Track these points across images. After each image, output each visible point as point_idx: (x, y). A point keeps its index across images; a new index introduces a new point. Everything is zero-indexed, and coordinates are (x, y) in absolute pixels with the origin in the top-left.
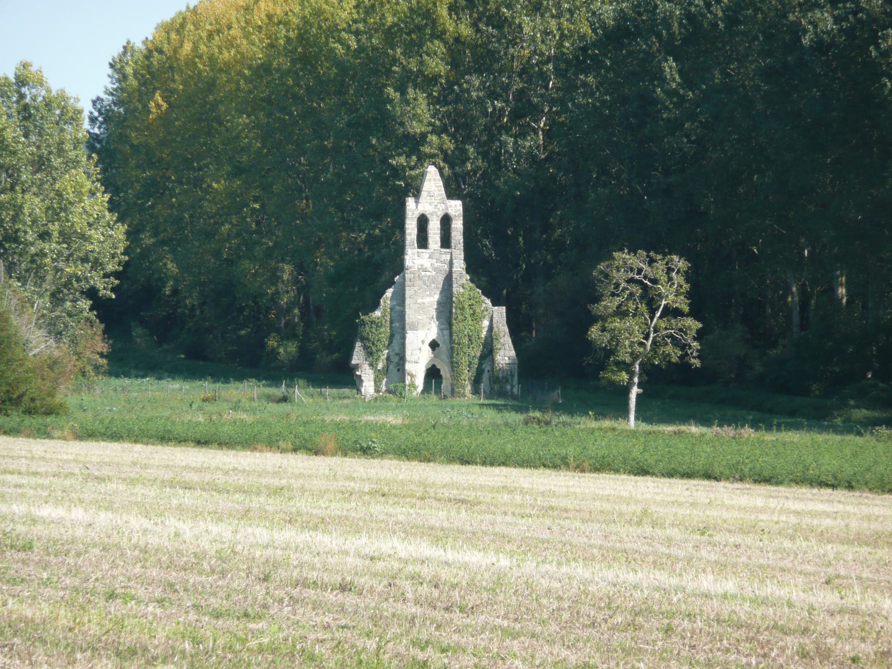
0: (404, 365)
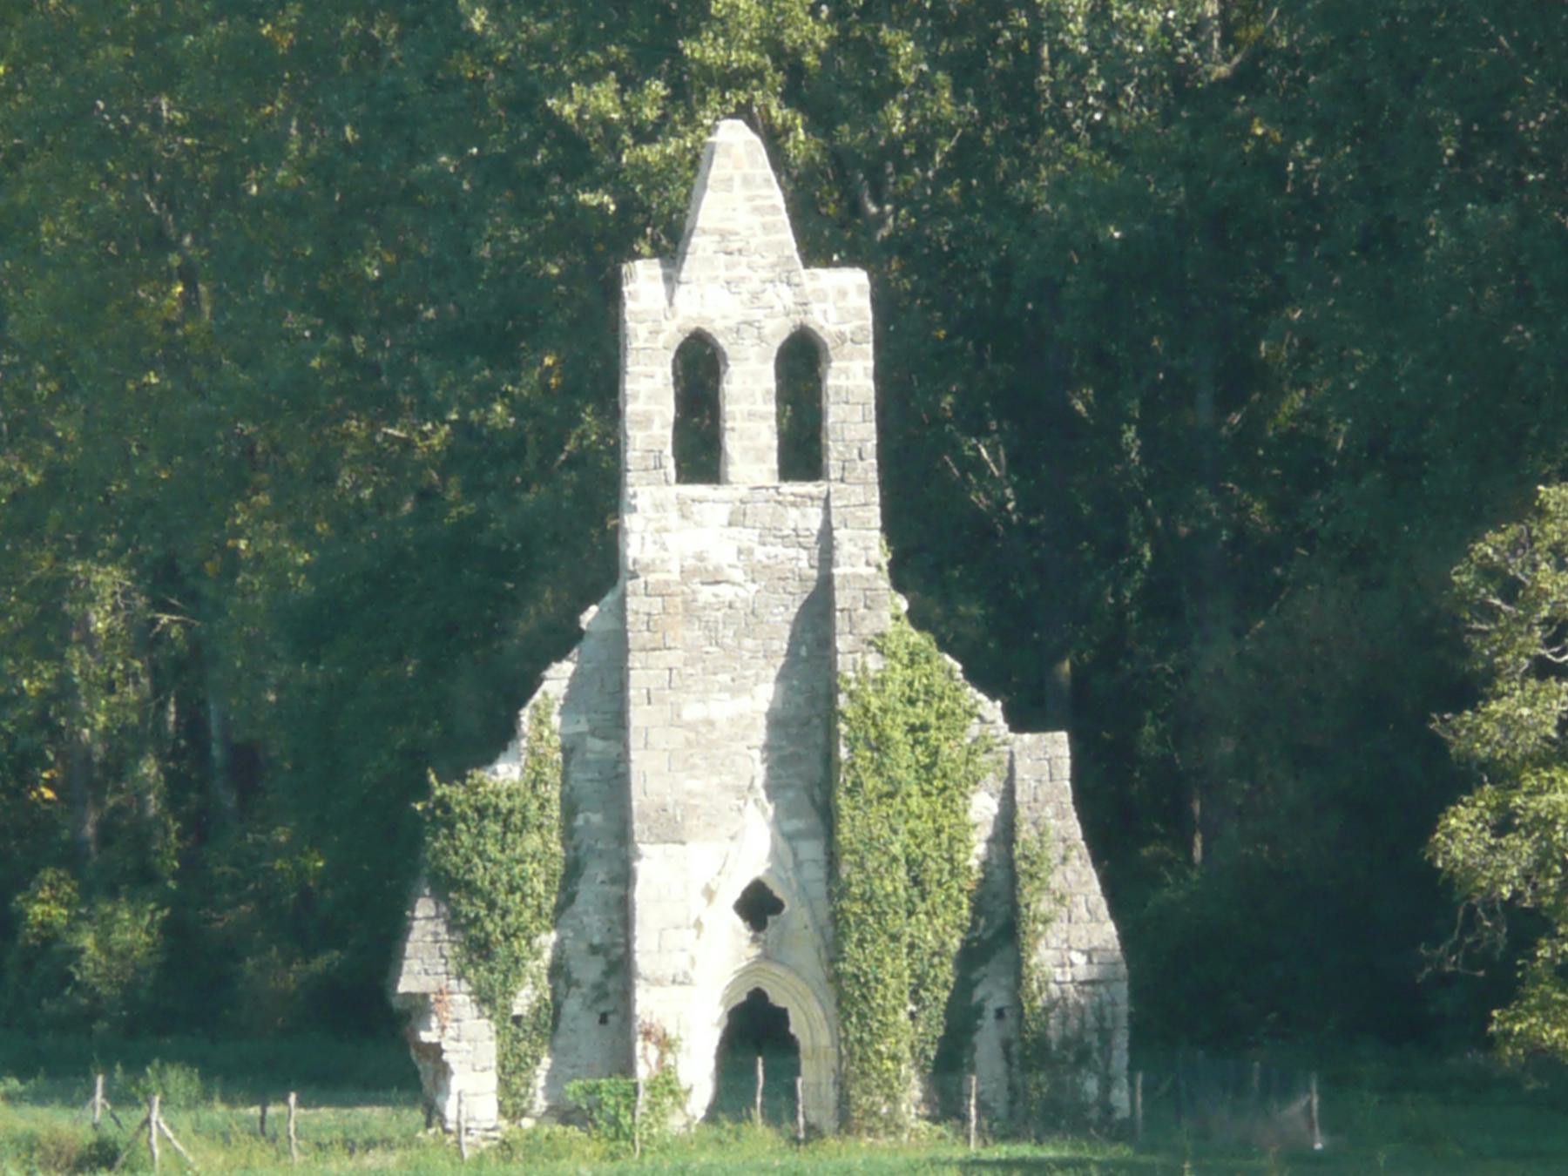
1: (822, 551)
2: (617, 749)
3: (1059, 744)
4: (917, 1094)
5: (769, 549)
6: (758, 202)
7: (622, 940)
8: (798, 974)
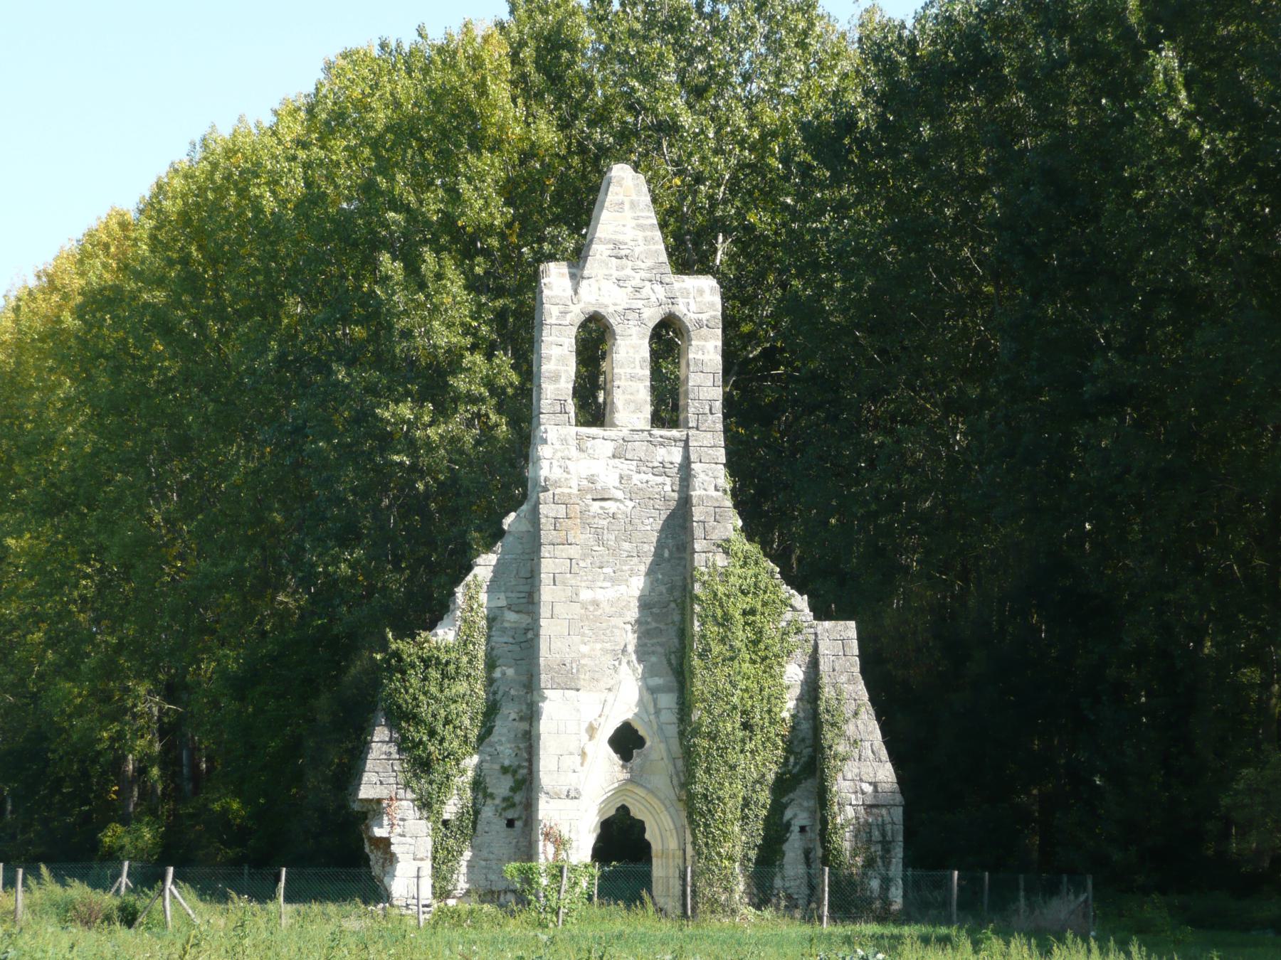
1: (682, 480)
2: (524, 620)
3: (849, 629)
4: (742, 887)
5: (644, 477)
6: (641, 221)
7: (526, 764)
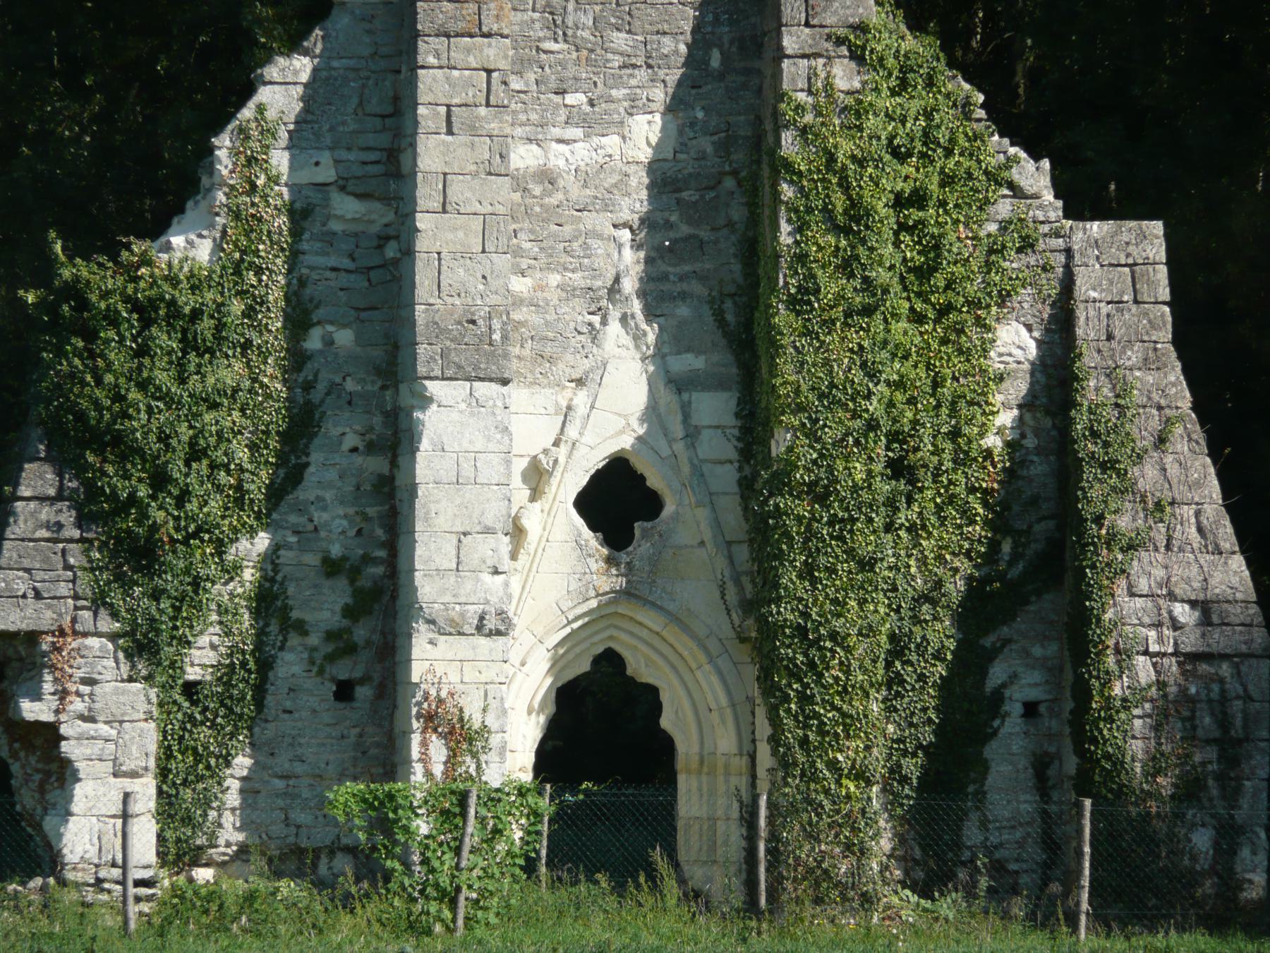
0: (390, 654)
2: (379, 215)
3: (1150, 241)
8: (686, 628)
